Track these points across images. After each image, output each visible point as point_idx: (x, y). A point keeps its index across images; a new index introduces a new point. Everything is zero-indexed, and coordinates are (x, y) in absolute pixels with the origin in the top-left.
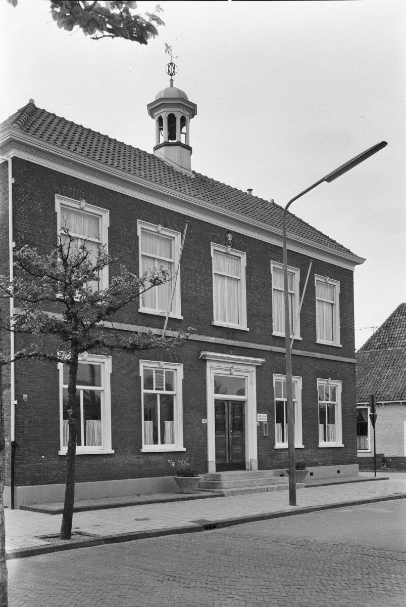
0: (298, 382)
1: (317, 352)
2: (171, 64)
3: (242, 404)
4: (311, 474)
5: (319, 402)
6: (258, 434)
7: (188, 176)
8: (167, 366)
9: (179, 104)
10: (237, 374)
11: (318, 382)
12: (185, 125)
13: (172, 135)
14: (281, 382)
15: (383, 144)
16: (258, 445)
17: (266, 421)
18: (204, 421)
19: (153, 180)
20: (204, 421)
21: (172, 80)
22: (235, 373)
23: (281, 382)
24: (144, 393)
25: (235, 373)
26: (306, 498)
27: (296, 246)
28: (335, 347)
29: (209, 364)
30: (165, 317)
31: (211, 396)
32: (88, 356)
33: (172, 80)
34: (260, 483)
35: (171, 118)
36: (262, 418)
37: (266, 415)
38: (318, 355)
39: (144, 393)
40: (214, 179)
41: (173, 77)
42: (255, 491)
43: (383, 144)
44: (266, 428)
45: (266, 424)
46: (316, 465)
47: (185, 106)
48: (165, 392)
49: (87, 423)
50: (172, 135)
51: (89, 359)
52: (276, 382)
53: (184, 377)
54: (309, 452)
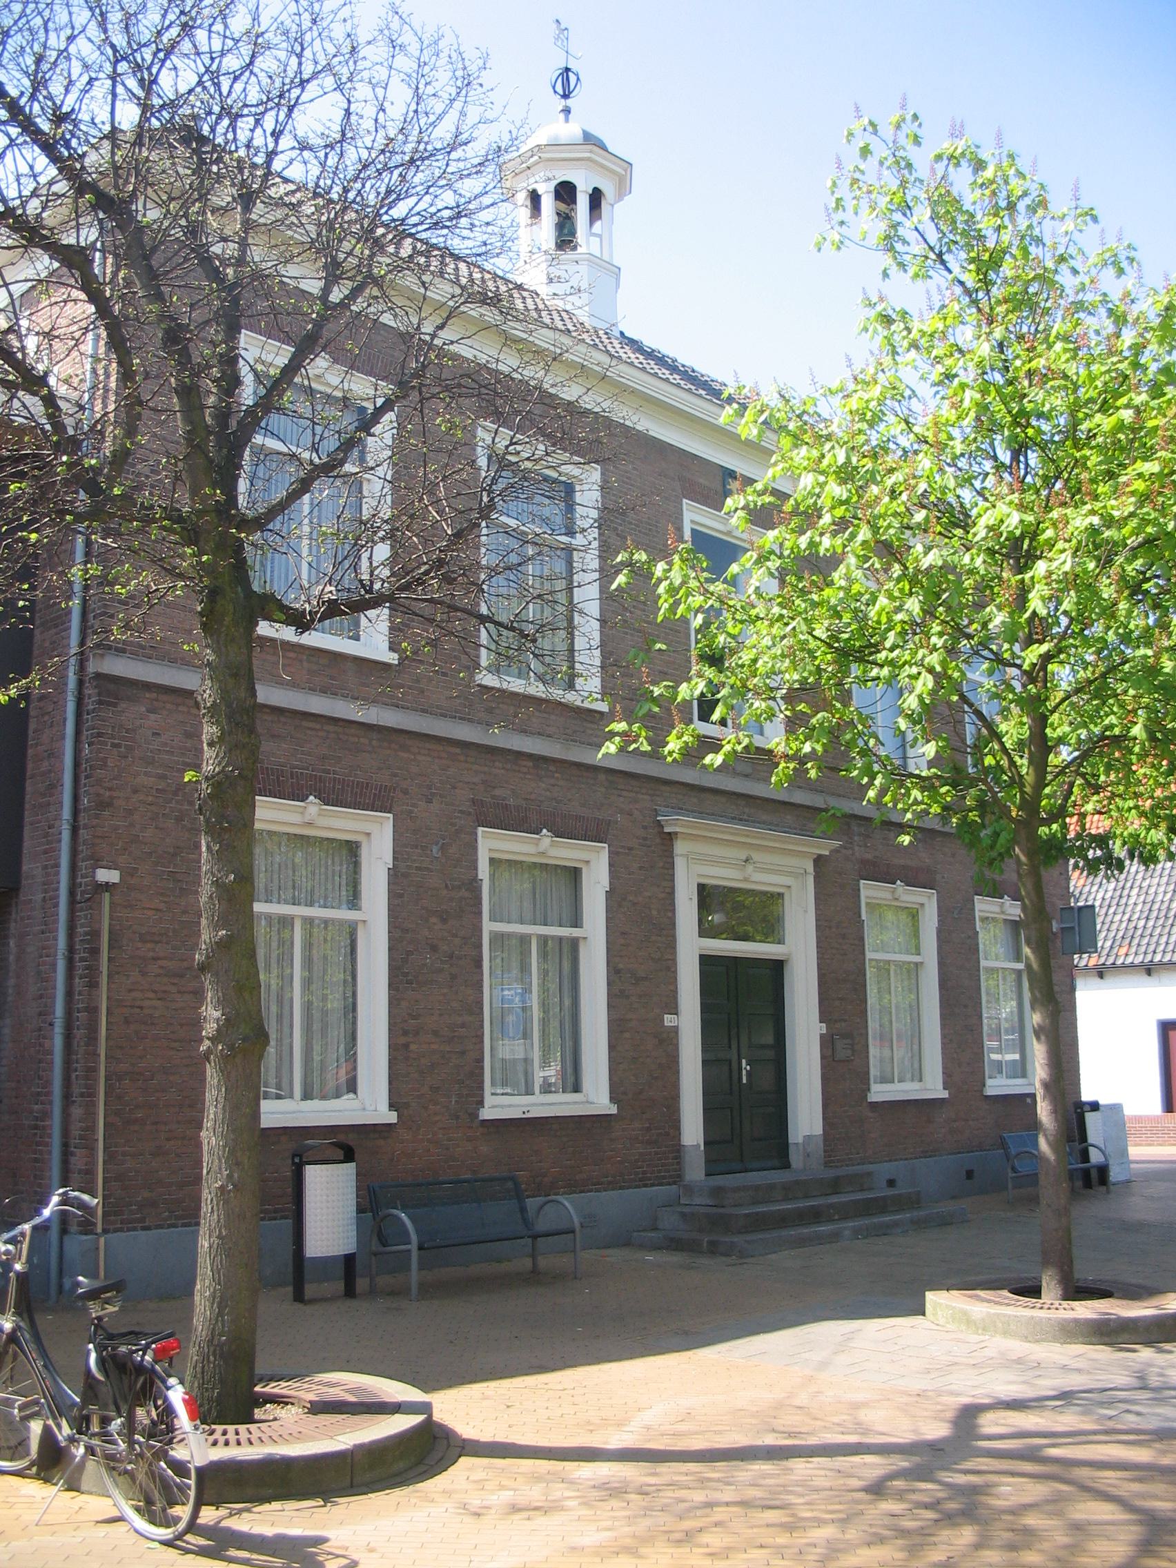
0: (927, 906)
2: (567, 70)
3: (777, 968)
6: (823, 1057)
8: (340, 822)
9: (588, 159)
11: (978, 906)
12: (600, 218)
16: (612, 1047)
18: (669, 1020)
19: (601, 332)
20: (669, 1020)
22: (758, 877)
24: (491, 932)
25: (758, 877)
29: (680, 847)
31: (690, 946)
32: (553, 844)
39: (491, 932)
41: (569, 102)
47: (602, 166)
51: (554, 852)
52: (867, 904)
53: (395, 858)
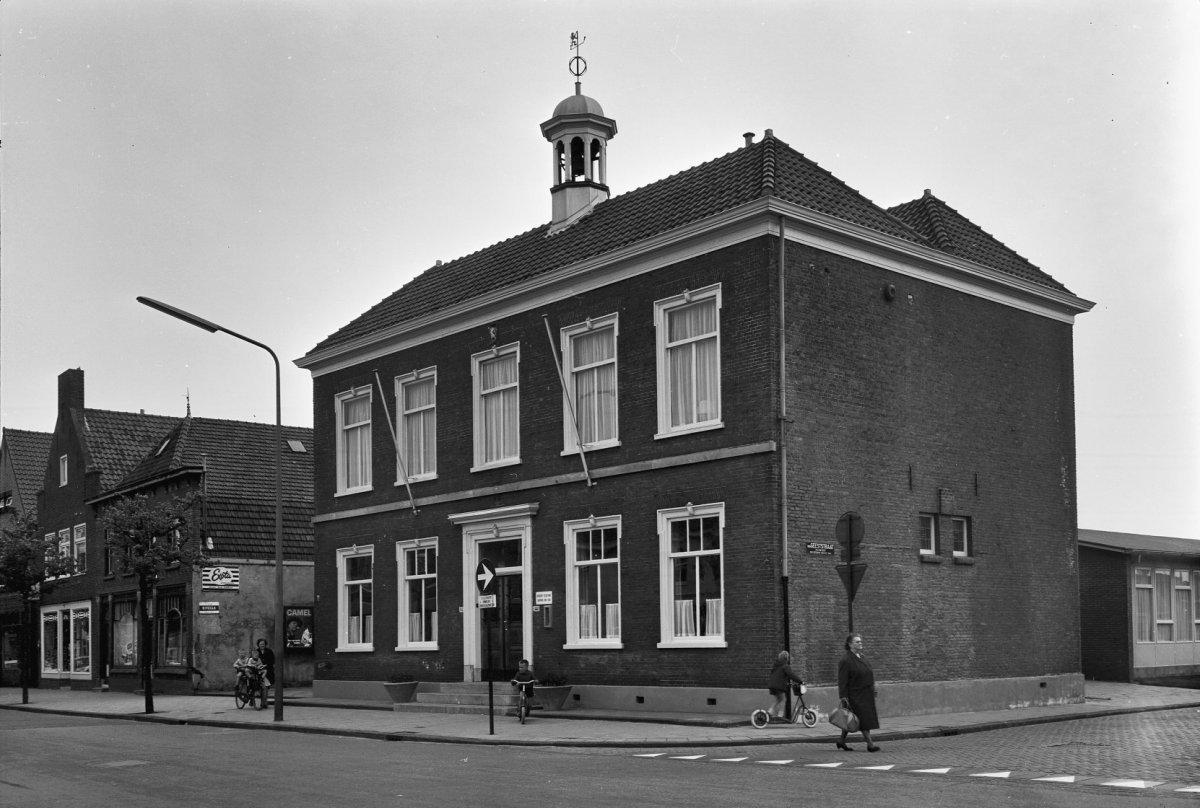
1: (652, 459)
4: (577, 697)
5: (370, 581)
7: (557, 233)
10: (507, 536)
13: (578, 168)
14: (685, 522)
15: (141, 300)
17: (551, 602)
21: (578, 84)
22: (502, 535)
23: (685, 522)
26: (292, 716)
27: (664, 255)
28: (668, 438)
29: (465, 530)
30: (578, 455)
33: (578, 84)
34: (463, 701)
35: (577, 145)
36: (543, 598)
37: (550, 593)
38: (656, 463)
40: (631, 191)
42: (453, 711)
43: (141, 300)
44: (547, 616)
45: (547, 609)
46: (655, 682)
48: (603, 561)
49: (709, 607)
50: (578, 168)
54: (638, 657)
